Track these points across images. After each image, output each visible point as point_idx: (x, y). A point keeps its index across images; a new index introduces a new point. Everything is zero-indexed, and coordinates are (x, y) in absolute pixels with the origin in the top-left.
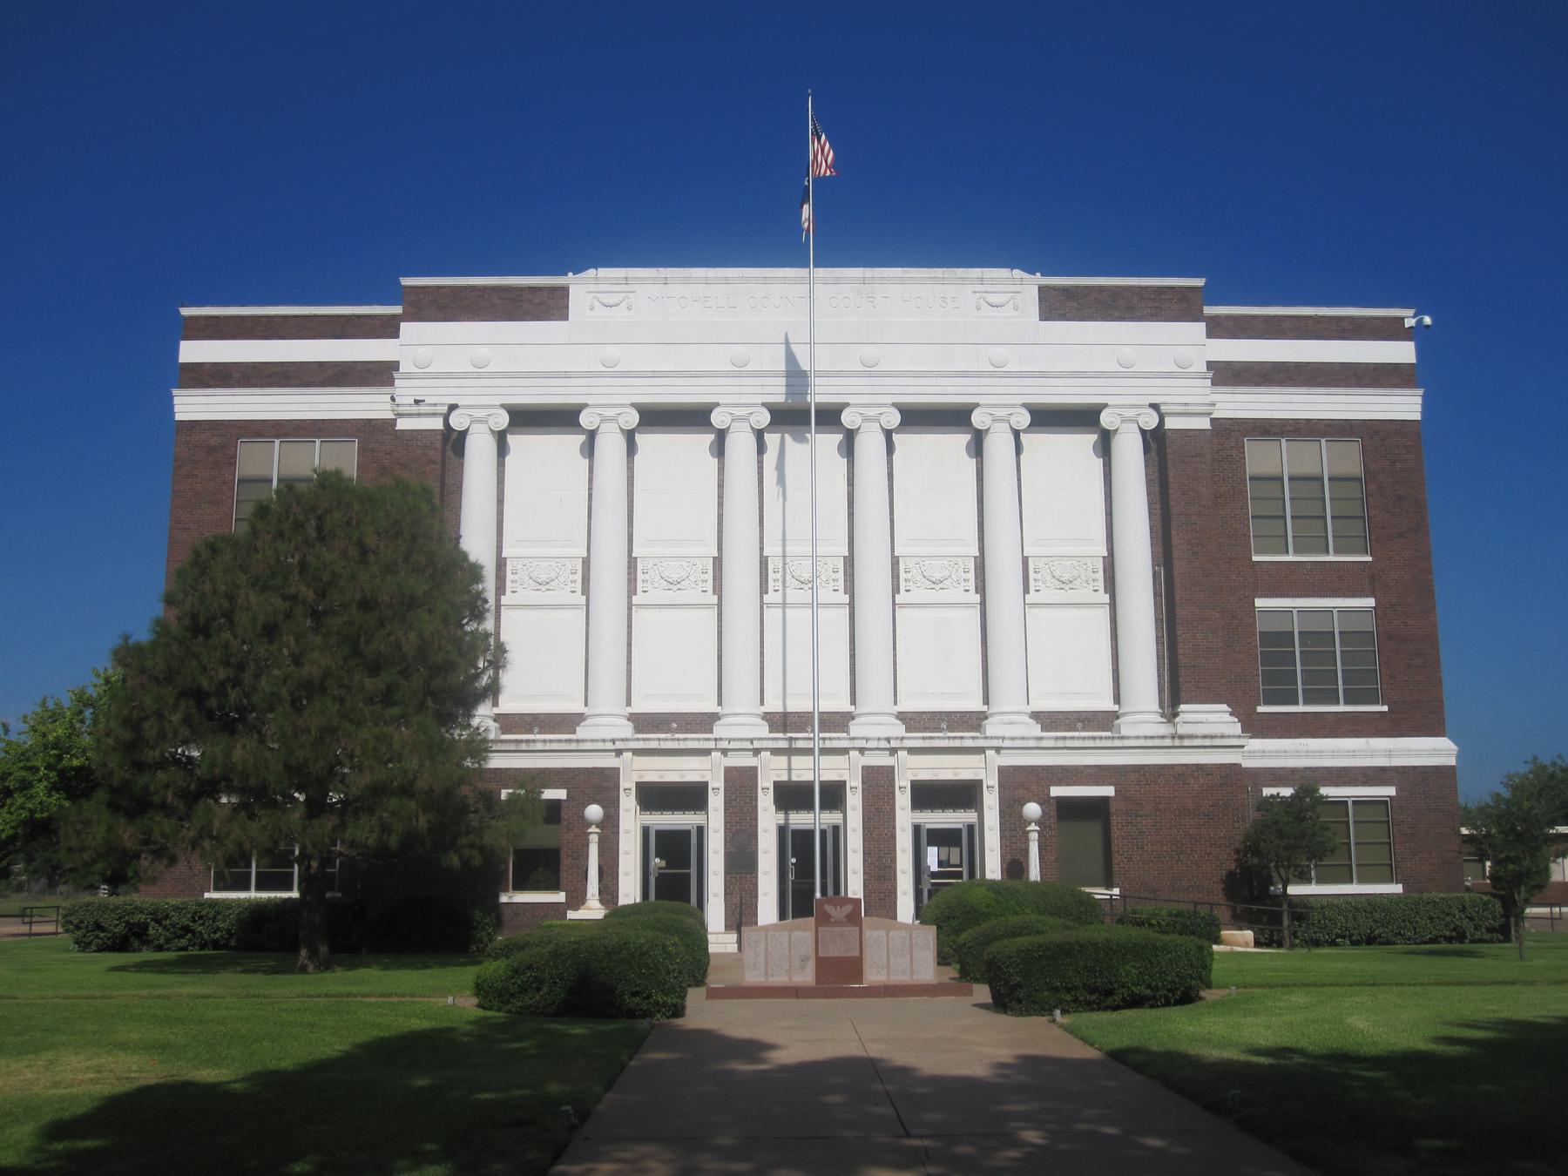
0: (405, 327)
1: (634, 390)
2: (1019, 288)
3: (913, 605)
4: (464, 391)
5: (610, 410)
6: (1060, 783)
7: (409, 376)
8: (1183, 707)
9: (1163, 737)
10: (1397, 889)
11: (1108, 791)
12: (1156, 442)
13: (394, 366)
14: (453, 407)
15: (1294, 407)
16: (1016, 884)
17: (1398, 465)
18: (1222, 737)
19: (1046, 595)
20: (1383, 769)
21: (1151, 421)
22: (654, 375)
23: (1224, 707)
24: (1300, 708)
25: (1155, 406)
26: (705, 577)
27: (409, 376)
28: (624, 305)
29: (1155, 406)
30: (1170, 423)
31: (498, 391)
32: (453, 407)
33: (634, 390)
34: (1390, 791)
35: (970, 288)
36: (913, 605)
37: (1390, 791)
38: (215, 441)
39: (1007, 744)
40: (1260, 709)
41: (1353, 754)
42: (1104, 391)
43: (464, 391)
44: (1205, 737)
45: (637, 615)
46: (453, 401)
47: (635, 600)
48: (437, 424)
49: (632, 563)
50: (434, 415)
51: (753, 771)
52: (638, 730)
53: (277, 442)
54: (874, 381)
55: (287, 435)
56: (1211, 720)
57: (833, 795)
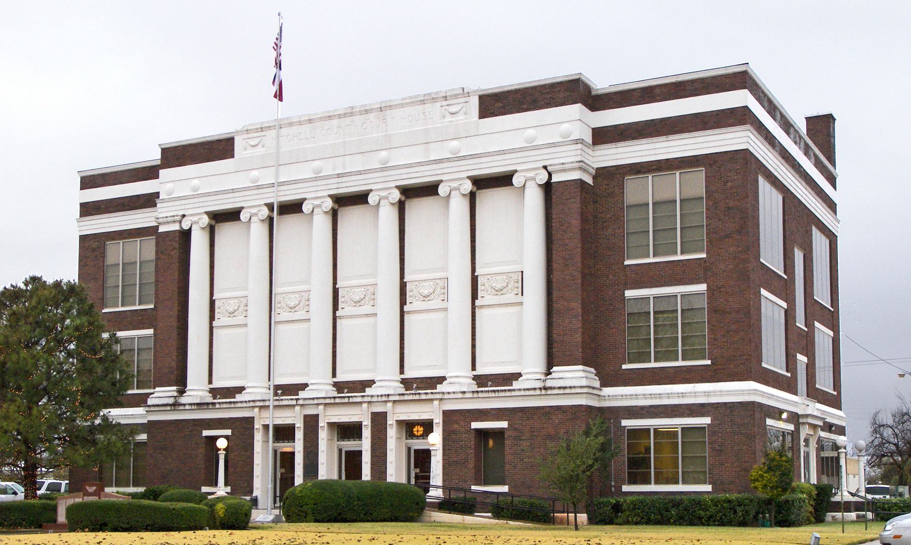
0: (162, 172)
1: (264, 196)
2: (467, 99)
3: (351, 317)
4: (187, 207)
5: (254, 209)
6: (476, 420)
7: (164, 201)
8: (555, 369)
9: (535, 389)
10: (708, 488)
11: (504, 424)
12: (548, 188)
13: (157, 195)
14: (184, 216)
15: (657, 152)
16: (351, 483)
17: (730, 184)
18: (571, 387)
19: (285, 315)
20: (703, 405)
21: (543, 177)
22: (503, 152)
23: (593, 370)
24: (653, 365)
25: (545, 167)
26: (483, 288)
27: (164, 201)
28: (462, 112)
29: (545, 167)
30: (555, 178)
31: (201, 204)
32: (184, 216)
33: (264, 196)
34: (707, 420)
35: (438, 104)
36: (351, 317)
37: (707, 420)
38: (95, 245)
39: (375, 399)
40: (624, 367)
41: (707, 394)
42: (514, 161)
43: (187, 207)
44: (560, 388)
45: (478, 312)
46: (181, 213)
47: (478, 303)
48: (176, 227)
49: (212, 303)
50: (174, 222)
51: (384, 415)
52: (479, 386)
53: (139, 240)
54: (386, 173)
55: (125, 238)
56: (575, 377)
57: (428, 426)
